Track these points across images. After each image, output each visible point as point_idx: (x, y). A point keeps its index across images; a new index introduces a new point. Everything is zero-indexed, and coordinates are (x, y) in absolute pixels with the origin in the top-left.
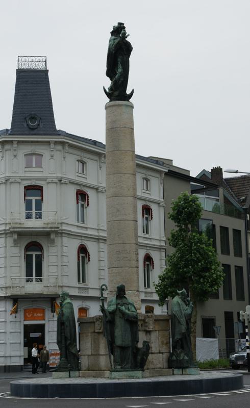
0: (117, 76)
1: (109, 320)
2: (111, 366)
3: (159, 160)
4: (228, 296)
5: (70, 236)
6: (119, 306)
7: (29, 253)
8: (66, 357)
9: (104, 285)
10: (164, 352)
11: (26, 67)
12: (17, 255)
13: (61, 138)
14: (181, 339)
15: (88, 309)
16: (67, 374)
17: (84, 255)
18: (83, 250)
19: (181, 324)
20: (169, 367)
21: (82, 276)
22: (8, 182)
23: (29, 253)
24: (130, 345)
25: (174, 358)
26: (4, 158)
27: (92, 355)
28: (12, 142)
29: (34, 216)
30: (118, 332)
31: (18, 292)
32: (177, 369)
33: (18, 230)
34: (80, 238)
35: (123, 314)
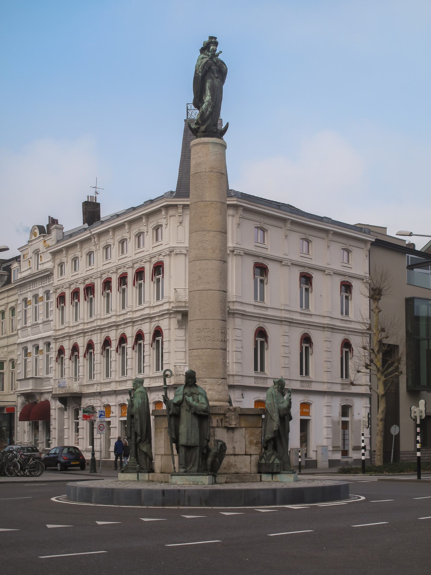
0: (204, 106)
1: (174, 414)
3: (363, 227)
5: (245, 317)
9: (167, 370)
10: (253, 453)
14: (273, 439)
15: (311, 404)
18: (261, 333)
19: (273, 420)
20: (260, 472)
22: (173, 254)
24: (198, 444)
25: (263, 461)
26: (168, 226)
27: (165, 455)
28: (176, 206)
30: (183, 428)
32: (266, 475)
34: (258, 319)
35: (190, 406)
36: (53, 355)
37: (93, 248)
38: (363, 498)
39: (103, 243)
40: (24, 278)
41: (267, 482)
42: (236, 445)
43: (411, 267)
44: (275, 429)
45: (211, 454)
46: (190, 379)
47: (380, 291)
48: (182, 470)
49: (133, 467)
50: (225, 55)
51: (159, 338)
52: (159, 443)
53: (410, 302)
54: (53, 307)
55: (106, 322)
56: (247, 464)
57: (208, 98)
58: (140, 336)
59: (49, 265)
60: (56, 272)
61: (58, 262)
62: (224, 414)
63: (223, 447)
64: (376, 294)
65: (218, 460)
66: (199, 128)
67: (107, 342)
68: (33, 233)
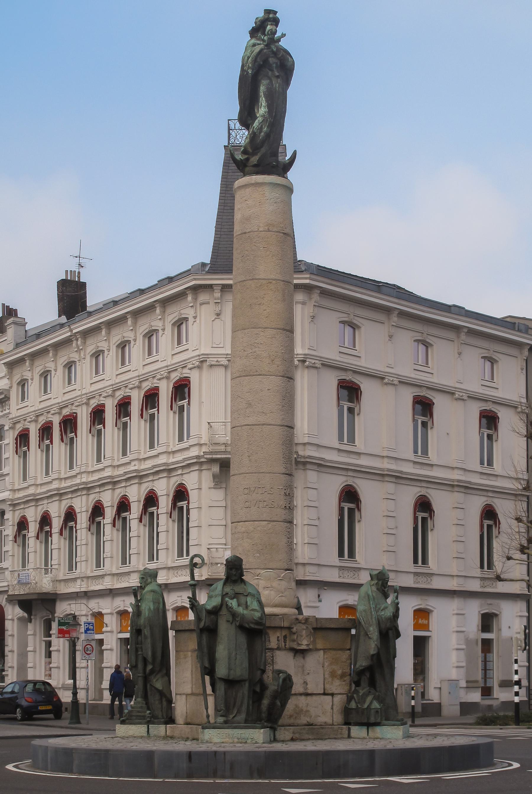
0: (256, 124)
1: (207, 627)
2: (208, 716)
3: (517, 321)
6: (227, 599)
12: (219, 504)
13: (306, 278)
14: (370, 669)
17: (425, 515)
18: (350, 495)
19: (370, 638)
21: (420, 553)
22: (205, 365)
24: (246, 676)
25: (353, 705)
26: (198, 320)
28: (210, 287)
30: (222, 651)
32: (357, 727)
33: (219, 456)
37: (75, 356)
38: (516, 765)
39: (91, 349)
41: (360, 740)
42: (309, 679)
44: (372, 652)
45: (268, 693)
46: (234, 570)
48: (221, 720)
49: (140, 714)
51: (184, 504)
52: (183, 676)
55: (96, 476)
56: (325, 710)
57: (262, 110)
58: (151, 500)
60: (14, 395)
61: (17, 378)
62: (289, 628)
63: (288, 681)
65: (278, 703)
66: (247, 160)
67: (98, 510)
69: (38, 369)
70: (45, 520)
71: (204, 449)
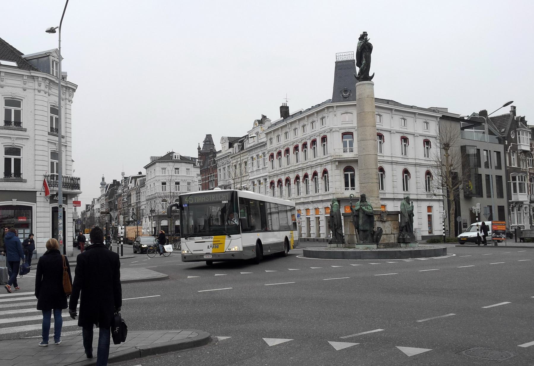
4: (489, 196)
7: (346, 173)
8: (336, 236)
11: (340, 60)
14: (406, 226)
16: (336, 245)
23: (346, 173)
29: (348, 150)
31: (340, 196)
35: (364, 211)
36: (268, 185)
37: (288, 130)
38: (454, 255)
39: (293, 128)
40: (251, 147)
41: (403, 248)
43: (463, 129)
45: (376, 234)
47: (449, 145)
50: (371, 40)
51: (326, 175)
52: (346, 230)
53: (463, 148)
54: (267, 161)
55: (297, 167)
56: (393, 239)
58: (315, 174)
59: (264, 140)
60: (268, 143)
61: (269, 138)
62: (380, 215)
64: (446, 146)
67: (297, 178)
68: (255, 123)
69: (276, 135)
70: (280, 181)
71: (333, 158)
